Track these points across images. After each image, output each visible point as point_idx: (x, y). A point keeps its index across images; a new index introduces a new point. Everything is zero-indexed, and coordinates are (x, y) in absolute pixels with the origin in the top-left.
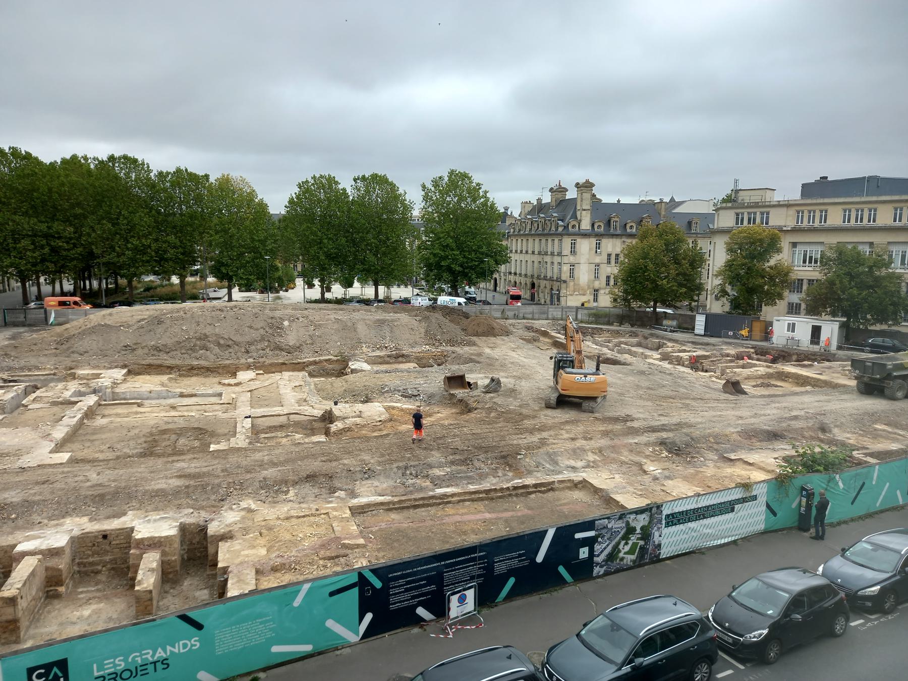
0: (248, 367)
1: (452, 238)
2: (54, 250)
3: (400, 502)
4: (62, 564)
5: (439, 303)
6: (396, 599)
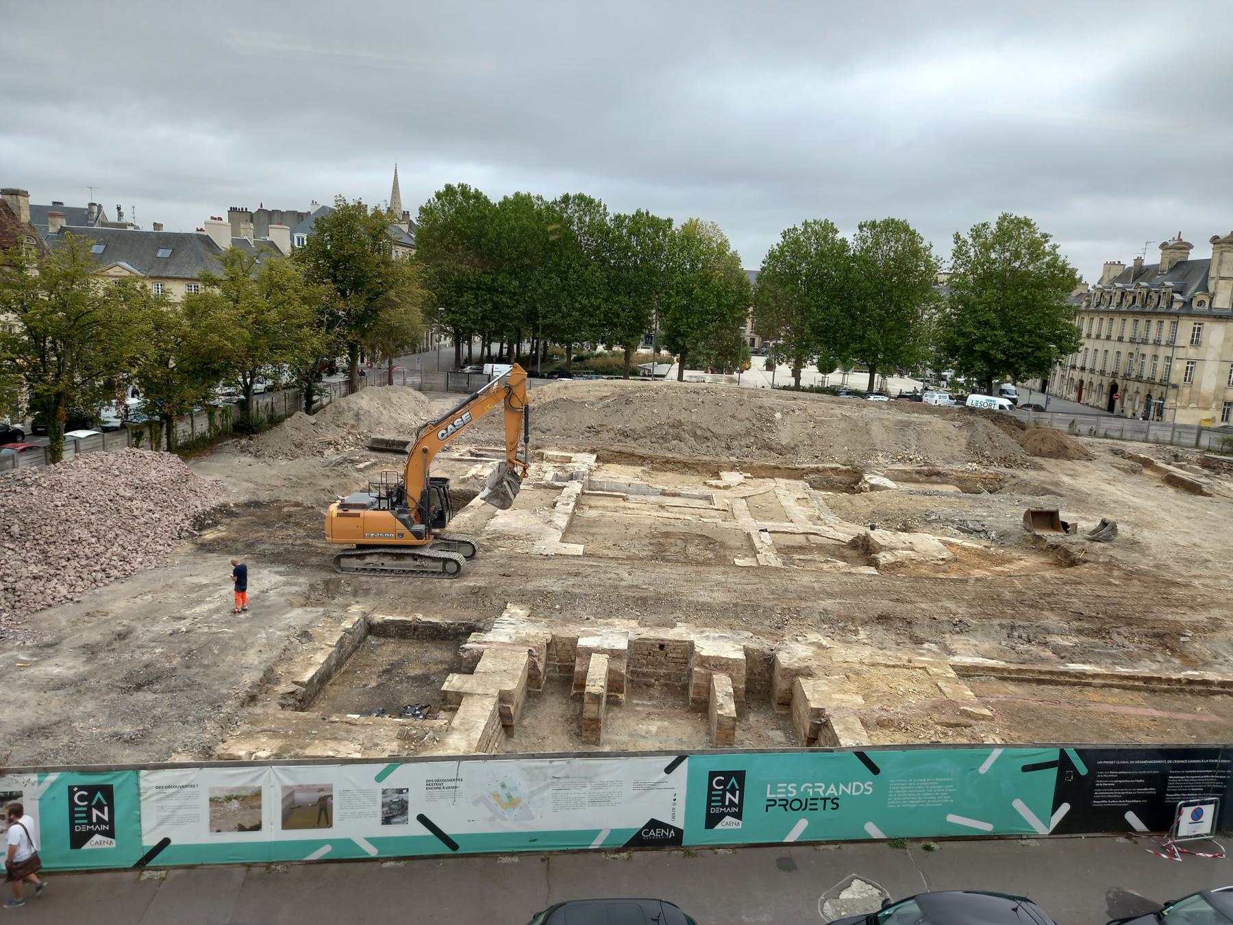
0: (733, 468)
1: (995, 311)
2: (496, 306)
3: (1019, 671)
4: (622, 667)
5: (968, 403)
6: (1103, 794)
